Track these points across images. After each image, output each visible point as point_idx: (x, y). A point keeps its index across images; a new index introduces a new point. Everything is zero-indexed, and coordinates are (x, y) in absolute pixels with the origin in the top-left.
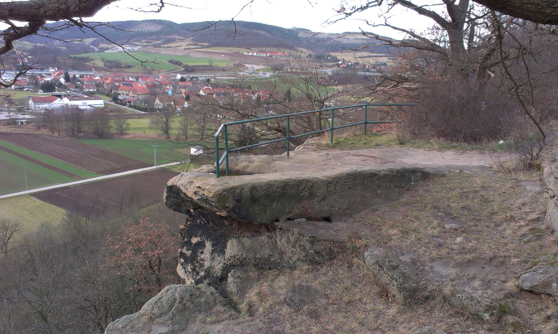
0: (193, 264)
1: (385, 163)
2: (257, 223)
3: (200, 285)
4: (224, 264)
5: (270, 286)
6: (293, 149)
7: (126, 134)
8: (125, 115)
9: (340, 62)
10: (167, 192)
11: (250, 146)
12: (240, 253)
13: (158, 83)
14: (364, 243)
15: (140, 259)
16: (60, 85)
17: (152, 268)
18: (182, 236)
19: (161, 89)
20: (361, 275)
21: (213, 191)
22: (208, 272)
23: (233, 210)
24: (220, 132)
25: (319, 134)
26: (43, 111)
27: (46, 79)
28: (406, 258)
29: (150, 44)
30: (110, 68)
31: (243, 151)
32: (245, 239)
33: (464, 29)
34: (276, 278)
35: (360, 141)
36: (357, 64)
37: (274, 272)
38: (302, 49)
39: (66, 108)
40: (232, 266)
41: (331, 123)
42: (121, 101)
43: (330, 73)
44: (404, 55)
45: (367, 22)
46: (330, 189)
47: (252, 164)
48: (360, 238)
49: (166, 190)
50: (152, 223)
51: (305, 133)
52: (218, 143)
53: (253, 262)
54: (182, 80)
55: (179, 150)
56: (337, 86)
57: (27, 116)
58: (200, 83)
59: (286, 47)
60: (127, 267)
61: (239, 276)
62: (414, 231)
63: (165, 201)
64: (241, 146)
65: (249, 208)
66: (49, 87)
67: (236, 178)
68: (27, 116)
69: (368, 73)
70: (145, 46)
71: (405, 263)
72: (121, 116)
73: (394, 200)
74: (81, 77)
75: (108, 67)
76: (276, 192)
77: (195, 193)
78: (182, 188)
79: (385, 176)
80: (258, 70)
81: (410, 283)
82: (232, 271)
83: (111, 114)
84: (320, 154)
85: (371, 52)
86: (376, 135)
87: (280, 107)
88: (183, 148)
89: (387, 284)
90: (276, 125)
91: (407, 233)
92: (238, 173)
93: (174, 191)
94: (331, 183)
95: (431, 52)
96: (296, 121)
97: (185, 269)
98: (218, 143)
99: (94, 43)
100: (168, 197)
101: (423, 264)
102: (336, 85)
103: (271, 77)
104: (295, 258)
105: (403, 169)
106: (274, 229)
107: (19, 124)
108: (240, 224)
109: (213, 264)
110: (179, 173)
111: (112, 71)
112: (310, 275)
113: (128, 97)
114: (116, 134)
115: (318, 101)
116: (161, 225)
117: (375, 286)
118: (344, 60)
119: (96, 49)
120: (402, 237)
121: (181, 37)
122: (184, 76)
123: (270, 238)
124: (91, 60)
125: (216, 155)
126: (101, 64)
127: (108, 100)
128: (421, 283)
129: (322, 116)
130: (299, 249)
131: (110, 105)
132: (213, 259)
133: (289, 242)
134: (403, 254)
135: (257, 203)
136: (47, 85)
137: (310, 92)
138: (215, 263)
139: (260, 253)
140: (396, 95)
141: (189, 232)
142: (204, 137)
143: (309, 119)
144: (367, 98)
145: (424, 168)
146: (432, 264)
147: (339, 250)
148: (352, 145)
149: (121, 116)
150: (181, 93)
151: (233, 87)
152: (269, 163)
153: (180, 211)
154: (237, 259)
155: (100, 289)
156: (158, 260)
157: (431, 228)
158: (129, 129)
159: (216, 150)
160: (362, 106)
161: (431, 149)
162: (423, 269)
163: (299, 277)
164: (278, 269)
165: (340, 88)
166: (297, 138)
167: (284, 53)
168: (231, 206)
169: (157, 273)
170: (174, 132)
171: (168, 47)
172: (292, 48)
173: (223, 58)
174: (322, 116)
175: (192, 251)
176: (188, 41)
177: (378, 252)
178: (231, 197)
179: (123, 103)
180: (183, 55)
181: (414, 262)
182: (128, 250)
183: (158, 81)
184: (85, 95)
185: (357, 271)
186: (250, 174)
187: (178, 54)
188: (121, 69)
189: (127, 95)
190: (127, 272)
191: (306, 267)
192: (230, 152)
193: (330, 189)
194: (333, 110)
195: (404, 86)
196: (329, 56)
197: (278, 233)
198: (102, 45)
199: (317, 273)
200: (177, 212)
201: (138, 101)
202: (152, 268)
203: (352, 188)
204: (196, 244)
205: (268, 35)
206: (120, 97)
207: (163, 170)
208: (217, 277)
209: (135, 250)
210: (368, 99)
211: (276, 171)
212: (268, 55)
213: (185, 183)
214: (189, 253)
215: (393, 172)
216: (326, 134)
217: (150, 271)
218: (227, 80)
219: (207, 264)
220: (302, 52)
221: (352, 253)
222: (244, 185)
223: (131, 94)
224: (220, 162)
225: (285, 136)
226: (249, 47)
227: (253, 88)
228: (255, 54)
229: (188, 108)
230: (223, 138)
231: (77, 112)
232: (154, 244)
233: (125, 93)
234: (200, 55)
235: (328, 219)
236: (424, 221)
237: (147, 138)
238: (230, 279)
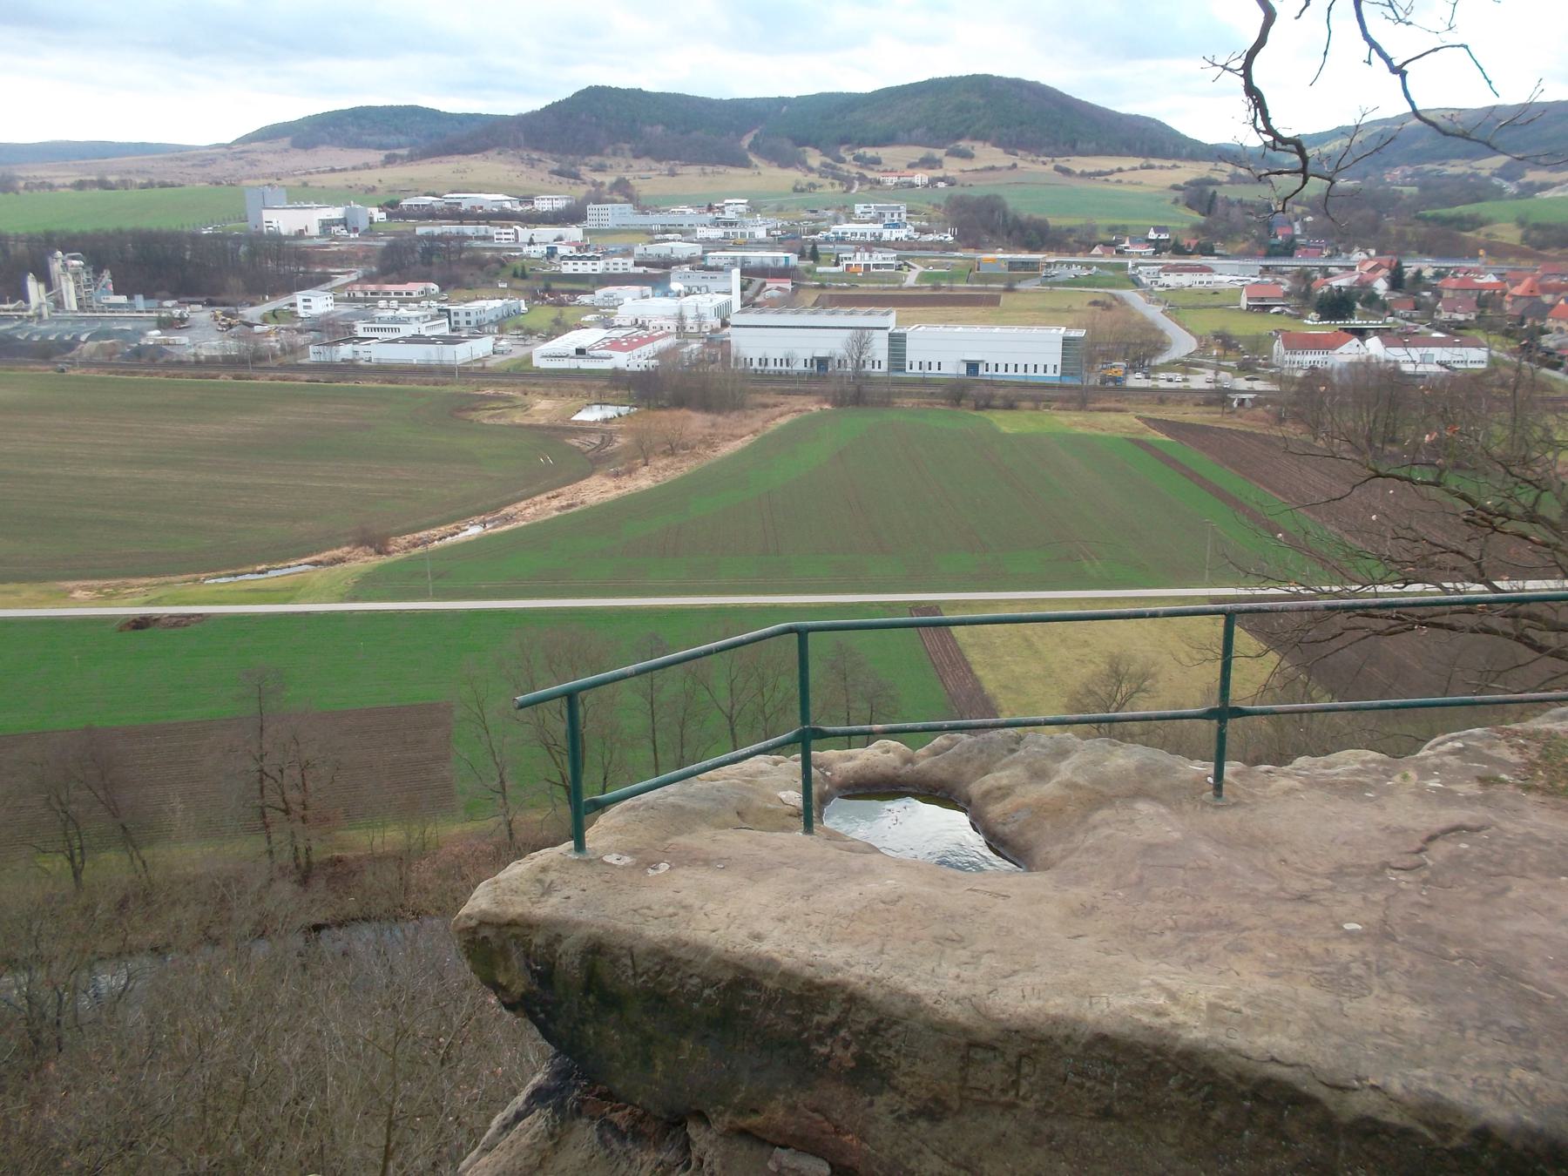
16: (1372, 300)
26: (1299, 374)
27: (1335, 283)
30: (1540, 248)
33: (1276, 388)
39: (1366, 367)
42: (1549, 353)
57: (1259, 386)
65: (583, 1021)
66: (1337, 306)
68: (1259, 386)
74: (1438, 275)
76: (695, 996)
79: (1368, 1130)
99: (1507, 173)
107: (1235, 404)
111: (1543, 258)
119: (1511, 188)
124: (1482, 225)
126: (1509, 234)
136: (1333, 298)
184: (1438, 330)
198: (1533, 176)
203: (1120, 1118)
215: (1444, 1130)
231: (1389, 387)
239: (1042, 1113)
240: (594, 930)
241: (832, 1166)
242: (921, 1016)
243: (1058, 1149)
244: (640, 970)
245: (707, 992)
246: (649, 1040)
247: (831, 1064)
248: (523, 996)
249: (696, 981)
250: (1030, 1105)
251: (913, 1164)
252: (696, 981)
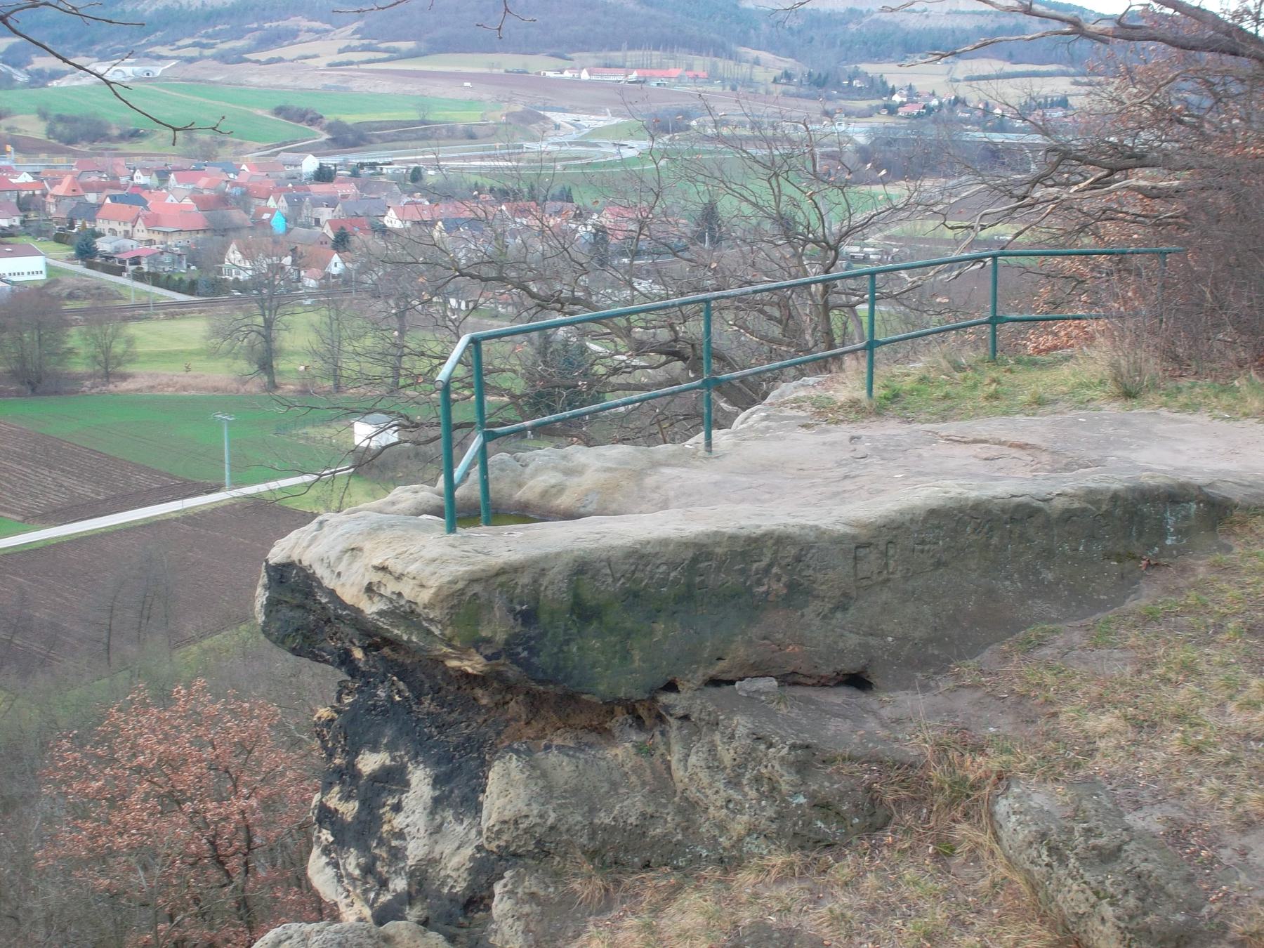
0: (364, 849)
1: (1068, 468)
2: (595, 699)
3: (391, 927)
4: (479, 848)
5: (648, 927)
6: (725, 422)
7: (124, 377)
8: (122, 309)
9: (897, 98)
10: (266, 588)
11: (567, 414)
12: (536, 808)
13: (236, 191)
14: (995, 765)
15: (177, 830)
17: (219, 862)
18: (325, 747)
19: (247, 212)
20: (984, 883)
21: (434, 583)
22: (421, 879)
23: (508, 650)
24: (460, 361)
25: (822, 365)
28: (1148, 821)
29: (207, 52)
30: (70, 142)
31: (544, 431)
32: (553, 758)
34: (669, 899)
35: (975, 387)
36: (958, 101)
37: (663, 879)
38: (755, 53)
40: (508, 857)
41: (866, 320)
42: (108, 257)
43: (861, 140)
44: (1129, 71)
46: (864, 569)
47: (573, 481)
48: (979, 749)
49: (263, 579)
50: (217, 697)
51: (770, 360)
52: (448, 403)
53: (584, 840)
54: (323, 175)
55: (310, 431)
56: (884, 184)
58: (385, 187)
59: (699, 46)
60: (133, 860)
61: (533, 895)
62: (1179, 718)
63: (261, 618)
64: (537, 412)
65: (567, 642)
67: (519, 532)
69: (997, 138)
70: (191, 60)
71: (1146, 838)
72: (106, 311)
73: (1101, 606)
75: (59, 137)
76: (663, 582)
77: (370, 589)
78: (320, 571)
79: (1068, 516)
80: (596, 132)
81: (1162, 910)
82: (508, 874)
83: (71, 305)
84: (829, 438)
85: (1011, 58)
86: (1035, 363)
87: (679, 267)
88: (327, 422)
89: (1080, 917)
90: (664, 335)
91: (1153, 725)
92: (524, 514)
93: (293, 584)
94: (869, 545)
95: (1227, 58)
96: (736, 318)
97: (336, 866)
98: (448, 403)
100: (271, 606)
101: (1214, 840)
102: (883, 181)
103: (641, 158)
104: (739, 825)
105: (1133, 490)
106: (660, 718)
108: (535, 703)
109: (438, 849)
110: (314, 516)
111: (75, 154)
112: (796, 886)
113: (129, 243)
114: (90, 377)
115: (815, 242)
116: (242, 713)
117: (1033, 926)
118: (910, 88)
119: (21, 77)
120: (1135, 743)
121: (317, 25)
122: (329, 161)
123: (644, 750)
125: (442, 449)
126: (36, 129)
127: (60, 256)
128: (1205, 911)
129: (833, 299)
130: (753, 794)
131: (68, 272)
132: (436, 831)
133: (714, 766)
134: (1138, 806)
135: (595, 624)
137: (785, 208)
138: (445, 847)
139: (609, 810)
140: (1107, 214)
141: (352, 731)
142: (402, 382)
143: (787, 307)
144: (1000, 228)
145: (1210, 485)
146: (1246, 841)
147: (903, 794)
148: (948, 403)
149: (106, 311)
150: (317, 221)
151: (504, 195)
152: (638, 475)
153: (315, 658)
154: (526, 831)
155: (39, 937)
156: (242, 835)
157: (1241, 707)
158: (132, 358)
159: (440, 431)
160: (979, 259)
161: (1235, 413)
162: (1212, 860)
163: (756, 895)
164: (676, 868)
165: (898, 191)
166: (743, 379)
167: (690, 68)
168: (501, 636)
169: (238, 880)
170: (292, 366)
171: (271, 61)
172: (719, 50)
173: (469, 95)
174: (833, 299)
175: (363, 803)
176: (345, 35)
177: (1046, 798)
178: (499, 603)
179: (112, 265)
180: (326, 87)
181: (1178, 834)
182: (134, 798)
183: (235, 184)
185: (971, 871)
186: (569, 515)
187: (306, 83)
188: (106, 145)
189: (127, 235)
190: (132, 879)
191: (779, 860)
192: (495, 436)
193: (864, 569)
194: (872, 274)
195: (1133, 182)
196: (856, 75)
197: (673, 734)
199: (822, 880)
200: (306, 661)
201: (166, 258)
202: (223, 864)
203: (945, 564)
204: (375, 778)
206: (103, 245)
207: (258, 505)
208: (453, 898)
209: (159, 796)
210: (1005, 231)
211: (664, 505)
212: (634, 76)
213: (333, 555)
214: (349, 809)
215: (1097, 503)
216: (849, 361)
217: (215, 874)
218: (480, 172)
219: (415, 850)
220: (757, 62)
221: (951, 804)
222: (546, 558)
223: (141, 233)
224: (458, 473)
225: (697, 369)
226: (561, 48)
227: (583, 198)
229: (346, 280)
230: (470, 386)
232: (226, 778)
233: (120, 229)
234: (386, 87)
235: (858, 681)
236: (1214, 680)
237: (198, 389)
238: (500, 906)
239: (906, 578)
240: (576, 553)
241: (776, 678)
242: (826, 537)
243: (918, 599)
244: (618, 575)
245: (673, 574)
246: (628, 634)
247: (771, 598)
248: (507, 643)
249: (663, 568)
250: (898, 575)
251: (841, 645)
252: (663, 568)
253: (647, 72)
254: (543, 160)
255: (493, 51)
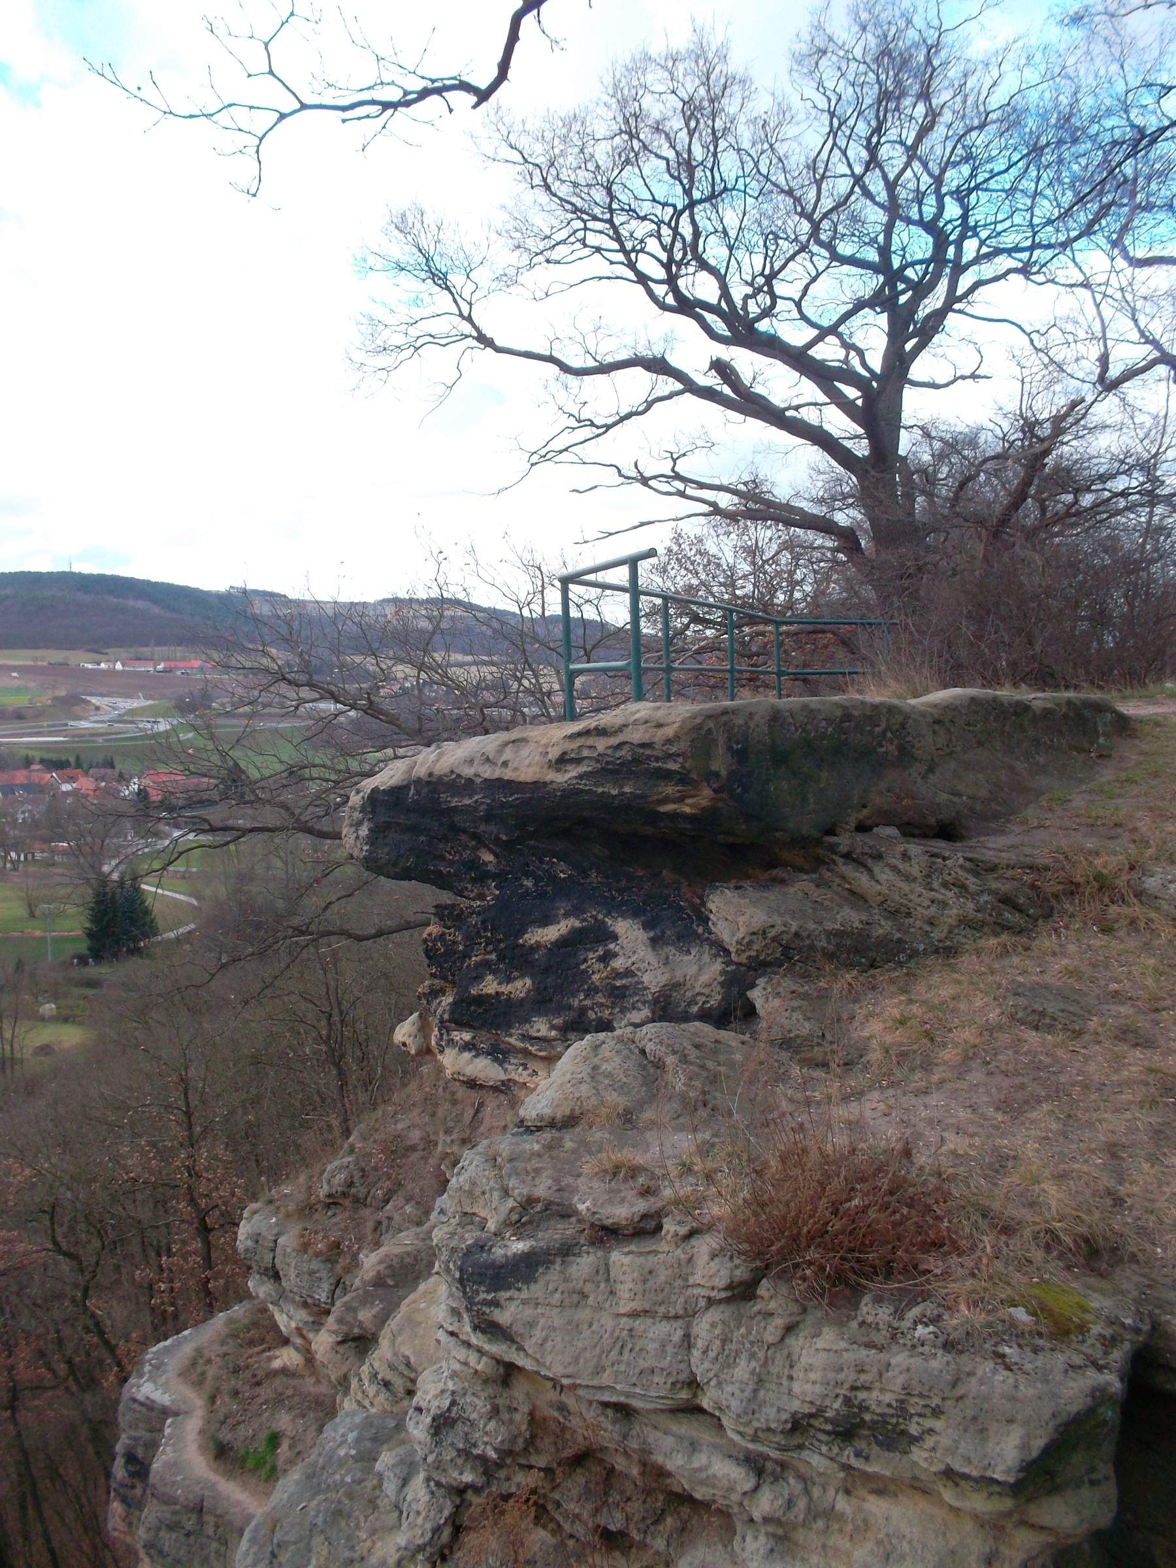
45: (619, 471)
80: (132, 712)
103: (174, 730)
154: (773, 940)
173: (16, 683)
178: (721, 741)
205: (156, 610)
212: (161, 667)
226: (98, 646)
228: (119, 666)
253: (173, 664)
254: (81, 736)
255: (37, 647)
